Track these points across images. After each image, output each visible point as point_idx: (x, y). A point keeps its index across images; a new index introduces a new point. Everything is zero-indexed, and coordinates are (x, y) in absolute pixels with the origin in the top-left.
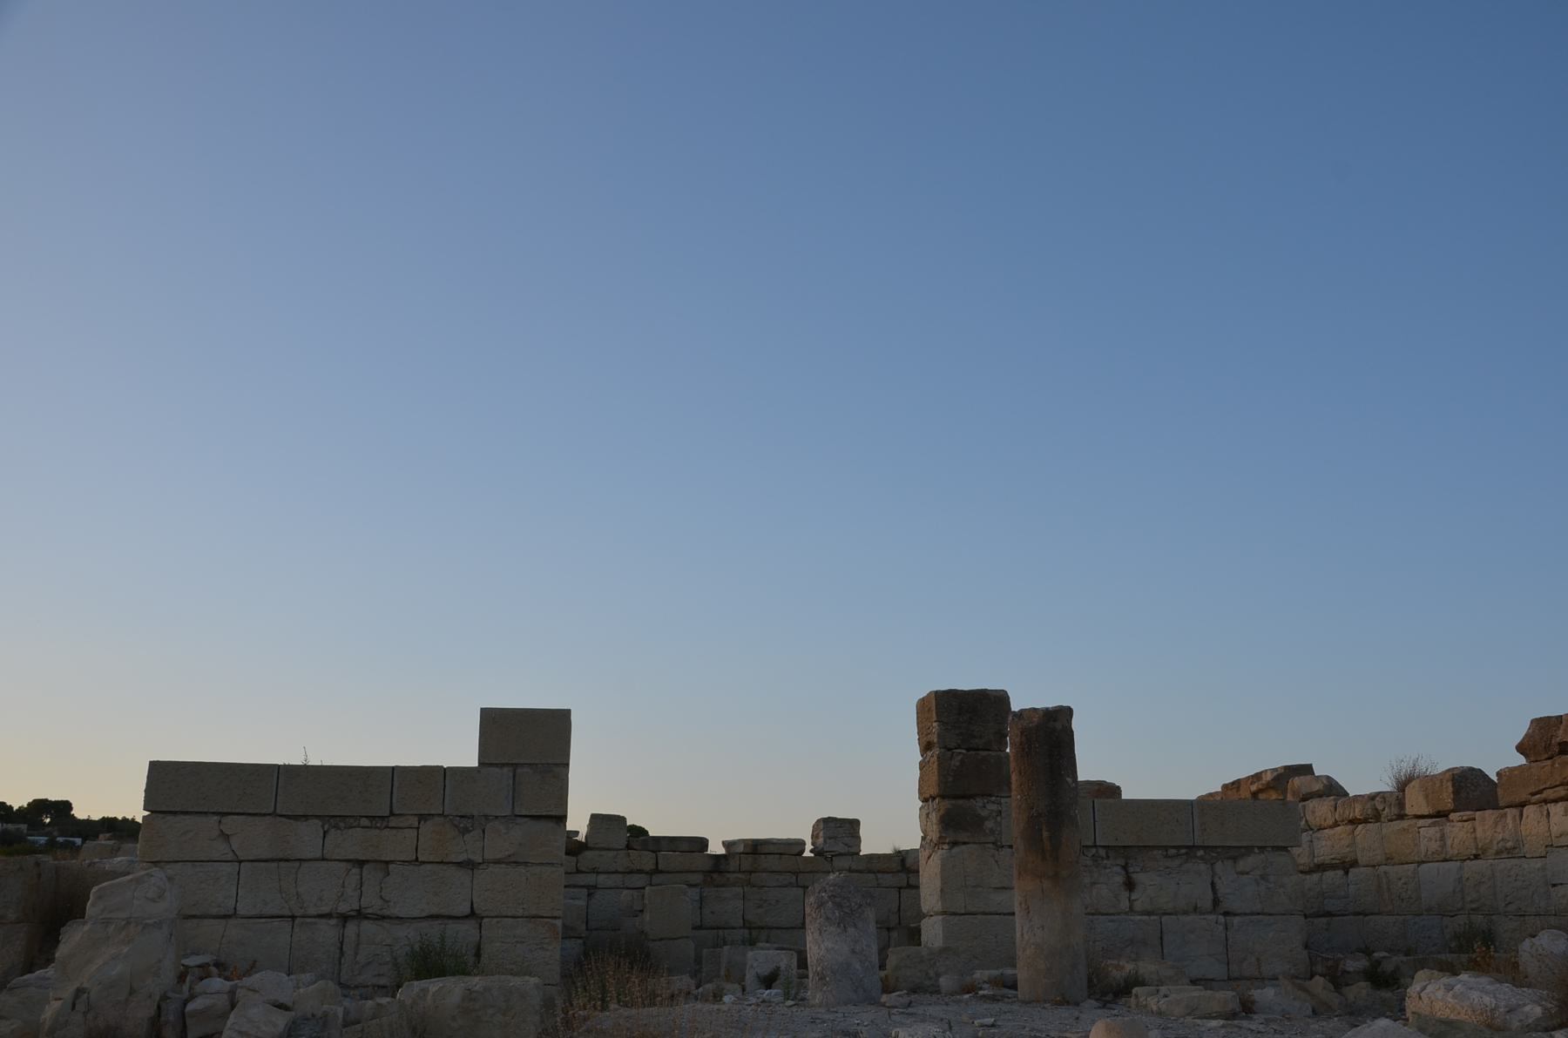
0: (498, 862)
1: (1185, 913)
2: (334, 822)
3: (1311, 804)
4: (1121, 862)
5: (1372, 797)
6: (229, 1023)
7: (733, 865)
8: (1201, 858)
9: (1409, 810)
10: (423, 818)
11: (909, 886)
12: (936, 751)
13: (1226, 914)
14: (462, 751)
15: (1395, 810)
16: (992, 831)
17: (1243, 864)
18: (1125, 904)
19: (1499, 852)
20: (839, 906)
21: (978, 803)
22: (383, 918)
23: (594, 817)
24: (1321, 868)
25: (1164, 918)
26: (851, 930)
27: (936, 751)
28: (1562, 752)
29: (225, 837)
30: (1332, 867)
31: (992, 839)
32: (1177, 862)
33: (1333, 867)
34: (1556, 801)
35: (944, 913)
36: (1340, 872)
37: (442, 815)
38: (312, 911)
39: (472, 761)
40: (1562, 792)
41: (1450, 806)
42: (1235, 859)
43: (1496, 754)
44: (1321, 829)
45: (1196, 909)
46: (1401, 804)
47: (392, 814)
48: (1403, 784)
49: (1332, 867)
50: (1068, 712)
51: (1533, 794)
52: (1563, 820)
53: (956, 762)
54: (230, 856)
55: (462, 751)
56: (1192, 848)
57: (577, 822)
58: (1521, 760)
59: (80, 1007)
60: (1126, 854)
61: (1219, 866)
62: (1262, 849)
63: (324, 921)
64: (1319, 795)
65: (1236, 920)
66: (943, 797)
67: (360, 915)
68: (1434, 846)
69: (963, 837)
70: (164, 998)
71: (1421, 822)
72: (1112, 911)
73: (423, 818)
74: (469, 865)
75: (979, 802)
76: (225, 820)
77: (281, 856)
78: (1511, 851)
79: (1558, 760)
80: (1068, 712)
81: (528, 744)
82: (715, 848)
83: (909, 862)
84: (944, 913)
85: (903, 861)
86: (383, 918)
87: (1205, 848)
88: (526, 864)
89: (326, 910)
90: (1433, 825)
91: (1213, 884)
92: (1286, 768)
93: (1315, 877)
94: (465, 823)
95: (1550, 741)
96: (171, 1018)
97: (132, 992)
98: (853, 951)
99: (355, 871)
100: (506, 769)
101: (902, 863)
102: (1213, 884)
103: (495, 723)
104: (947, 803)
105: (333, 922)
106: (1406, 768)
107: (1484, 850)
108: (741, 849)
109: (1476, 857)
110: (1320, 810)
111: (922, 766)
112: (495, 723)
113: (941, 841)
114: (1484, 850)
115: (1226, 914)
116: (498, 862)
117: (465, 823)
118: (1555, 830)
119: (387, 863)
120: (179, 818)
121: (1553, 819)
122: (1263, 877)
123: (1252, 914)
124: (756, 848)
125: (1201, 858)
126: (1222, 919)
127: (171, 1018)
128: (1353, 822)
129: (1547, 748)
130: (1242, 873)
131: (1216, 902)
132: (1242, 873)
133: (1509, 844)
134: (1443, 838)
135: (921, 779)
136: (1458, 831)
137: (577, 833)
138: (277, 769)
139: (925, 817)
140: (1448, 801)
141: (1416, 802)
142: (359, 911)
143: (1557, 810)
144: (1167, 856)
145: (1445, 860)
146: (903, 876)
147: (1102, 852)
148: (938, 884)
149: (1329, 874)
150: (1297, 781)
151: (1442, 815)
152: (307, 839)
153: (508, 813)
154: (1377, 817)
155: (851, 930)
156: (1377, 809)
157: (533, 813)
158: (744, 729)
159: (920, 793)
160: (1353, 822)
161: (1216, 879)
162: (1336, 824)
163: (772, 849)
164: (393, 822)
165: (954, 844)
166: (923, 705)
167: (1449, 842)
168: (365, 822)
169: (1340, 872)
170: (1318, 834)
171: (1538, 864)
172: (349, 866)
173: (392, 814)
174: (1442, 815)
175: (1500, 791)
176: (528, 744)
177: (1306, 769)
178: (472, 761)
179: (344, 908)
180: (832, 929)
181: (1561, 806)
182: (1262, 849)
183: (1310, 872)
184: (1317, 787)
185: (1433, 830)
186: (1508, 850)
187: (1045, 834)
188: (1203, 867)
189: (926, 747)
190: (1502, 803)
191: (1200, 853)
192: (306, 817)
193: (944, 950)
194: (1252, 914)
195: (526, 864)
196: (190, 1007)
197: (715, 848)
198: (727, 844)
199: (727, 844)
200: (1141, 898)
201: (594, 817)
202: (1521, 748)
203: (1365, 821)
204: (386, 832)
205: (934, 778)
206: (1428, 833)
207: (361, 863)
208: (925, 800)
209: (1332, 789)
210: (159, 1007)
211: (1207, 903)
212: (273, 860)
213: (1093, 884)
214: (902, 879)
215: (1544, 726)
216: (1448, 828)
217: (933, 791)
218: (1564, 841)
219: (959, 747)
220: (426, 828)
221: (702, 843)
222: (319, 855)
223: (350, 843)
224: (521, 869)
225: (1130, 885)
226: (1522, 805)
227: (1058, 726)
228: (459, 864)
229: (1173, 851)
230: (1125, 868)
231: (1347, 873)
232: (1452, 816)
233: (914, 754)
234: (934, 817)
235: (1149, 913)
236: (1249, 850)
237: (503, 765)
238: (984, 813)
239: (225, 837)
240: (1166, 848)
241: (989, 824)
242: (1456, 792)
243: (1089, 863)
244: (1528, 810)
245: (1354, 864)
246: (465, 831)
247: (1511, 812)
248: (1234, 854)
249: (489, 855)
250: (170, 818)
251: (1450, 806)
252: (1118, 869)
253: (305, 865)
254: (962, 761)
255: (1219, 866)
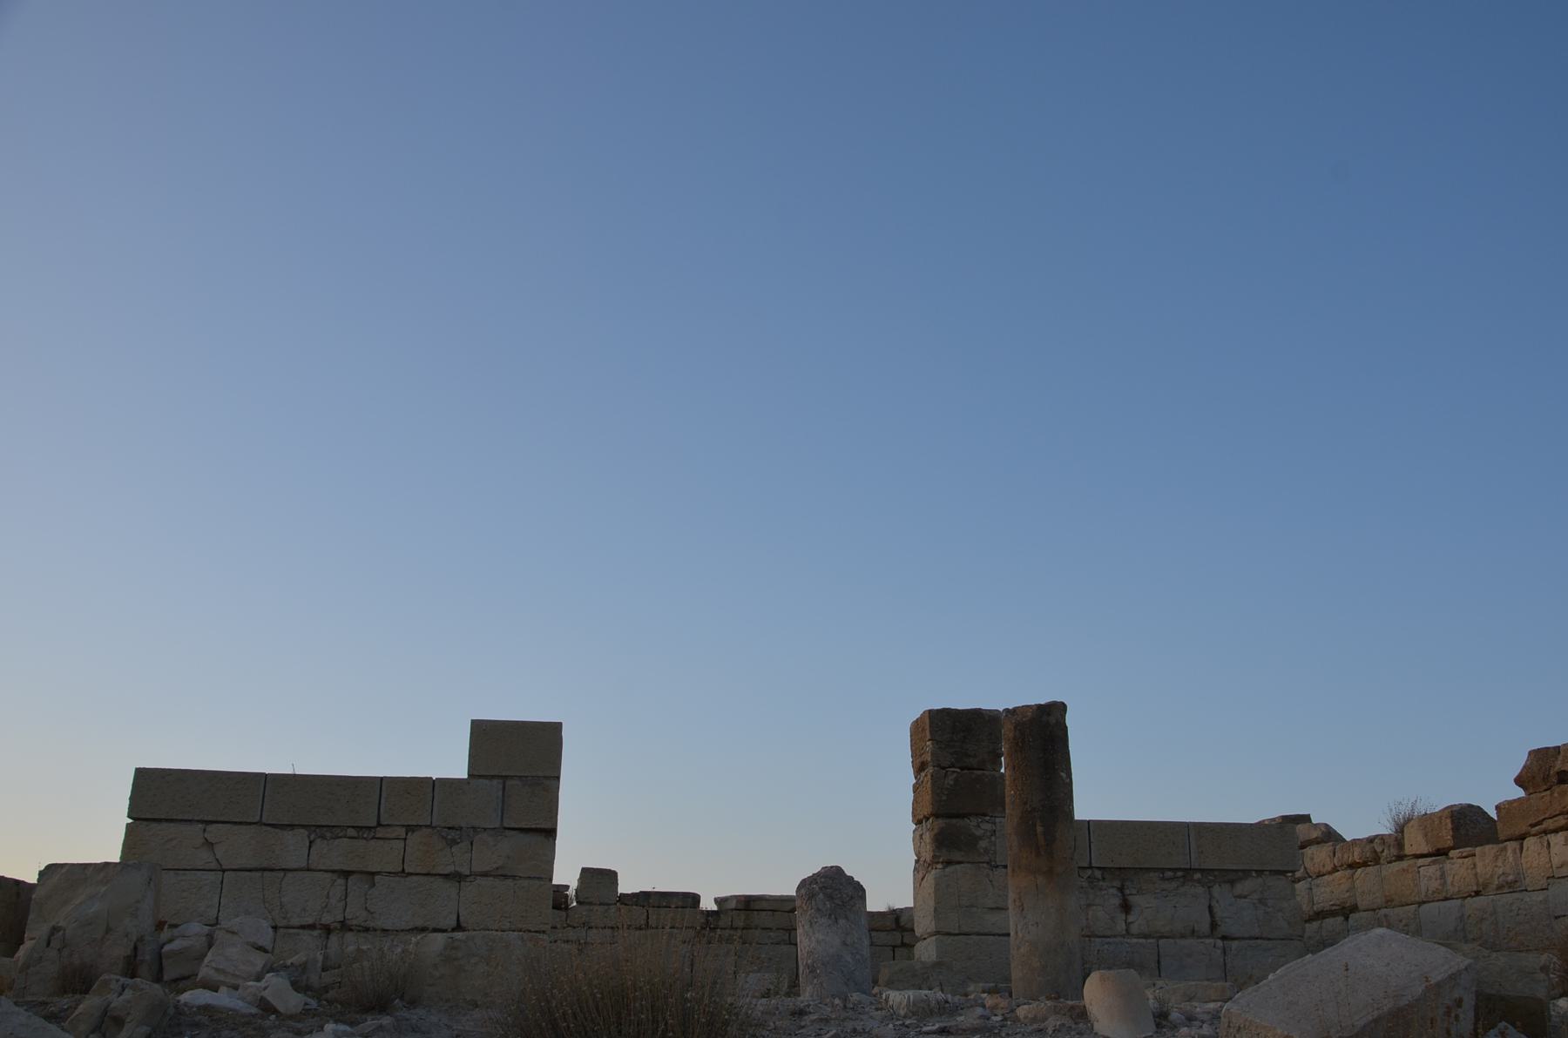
0: (485, 875)
1: (1183, 936)
2: (320, 831)
3: (1308, 851)
4: (1117, 883)
5: (1371, 840)
6: (206, 960)
7: (725, 921)
8: (1199, 881)
9: (1408, 850)
10: (410, 829)
11: (903, 945)
12: (930, 770)
13: (1224, 938)
14: (455, 765)
15: (1394, 851)
16: (986, 851)
17: (1240, 888)
18: (1121, 927)
19: (1500, 887)
20: (830, 898)
21: (972, 822)
22: (367, 930)
23: (584, 871)
24: (1320, 915)
25: (1162, 942)
26: (842, 922)
27: (930, 770)
28: (1561, 781)
29: (209, 845)
30: (1332, 914)
31: (986, 858)
32: (1174, 884)
33: (1332, 914)
34: (1556, 831)
35: (937, 933)
36: (1340, 919)
37: (429, 826)
38: (296, 921)
39: (460, 771)
40: (1562, 821)
41: (1450, 843)
42: (1232, 883)
43: (1493, 788)
44: (1320, 875)
45: (1193, 931)
46: (1400, 844)
47: (379, 824)
48: (1400, 829)
49: (1332, 914)
50: (1060, 708)
51: (1533, 826)
52: (1565, 850)
53: (950, 781)
54: (214, 865)
55: (455, 765)
56: (1188, 872)
57: (566, 874)
58: (1519, 793)
59: (55, 943)
60: (1122, 876)
61: (1216, 890)
62: (1260, 872)
63: (306, 932)
64: (1317, 841)
65: (1235, 944)
66: (936, 815)
67: (345, 926)
68: (1435, 884)
69: (957, 856)
70: (141, 939)
71: (1421, 861)
72: (1108, 933)
73: (410, 829)
74: (457, 877)
75: (973, 822)
76: (211, 828)
77: (265, 865)
78: (1512, 885)
79: (1557, 789)
80: (1060, 708)
81: (520, 760)
82: (708, 904)
83: (903, 920)
84: (937, 933)
85: (897, 920)
86: (367, 930)
87: (1202, 871)
88: (514, 877)
89: (310, 921)
90: (1434, 863)
91: (1210, 908)
92: (1284, 818)
93: (1315, 924)
94: (454, 835)
95: (1549, 772)
96: (148, 957)
97: (108, 930)
98: (844, 944)
99: (341, 881)
100: (495, 782)
101: (896, 921)
102: (1210, 908)
103: (486, 736)
104: (941, 822)
105: (316, 933)
106: (1405, 810)
107: (1485, 886)
108: (733, 905)
109: (1477, 893)
110: (1318, 857)
111: (916, 789)
112: (486, 736)
113: (935, 861)
114: (1485, 886)
115: (1224, 938)
116: (485, 875)
117: (454, 835)
118: (1556, 861)
119: (373, 874)
120: (164, 825)
121: (1554, 850)
122: (1260, 901)
123: (1251, 938)
124: (748, 904)
125: (1199, 881)
126: (1220, 943)
127: (148, 957)
128: (1353, 866)
129: (1546, 779)
130: (1240, 897)
131: (1214, 925)
132: (1240, 897)
133: (1511, 878)
134: (1443, 876)
135: (915, 802)
136: (1458, 869)
137: (567, 887)
138: (265, 777)
139: (918, 838)
140: (1447, 838)
141: (1415, 843)
142: (343, 923)
143: (1557, 840)
144: (1163, 879)
145: (1446, 899)
146: (898, 935)
147: (1098, 874)
148: (932, 903)
149: (1329, 921)
150: (1300, 827)
151: (1441, 853)
152: (292, 849)
153: (497, 825)
154: (1376, 859)
155: (842, 922)
156: (1374, 852)
157: (523, 825)
158: (736, 785)
159: (914, 815)
160: (1353, 866)
161: (1214, 903)
162: (1335, 870)
163: (765, 905)
164: (381, 832)
165: (948, 863)
166: (917, 728)
167: (1449, 880)
168: (351, 832)
169: (1340, 919)
170: (1318, 881)
171: (1540, 896)
172: (335, 876)
173: (379, 824)
174: (1441, 853)
175: (1499, 826)
176: (520, 760)
177: (1305, 819)
178: (460, 771)
179: (327, 919)
180: (824, 920)
181: (1561, 836)
182: (1260, 872)
183: (1310, 920)
184: (1314, 834)
185: (1432, 869)
186: (1510, 884)
187: (1039, 829)
188: (1200, 890)
189: (919, 768)
190: (1502, 837)
191: (1197, 876)
192: (292, 826)
193: (938, 965)
194: (1251, 938)
195: (514, 877)
196: (167, 948)
197: (708, 904)
198: (718, 901)
199: (718, 901)
200: (1138, 922)
201: (584, 871)
202: (1519, 781)
203: (1365, 864)
204: (373, 842)
205: (928, 797)
206: (1429, 872)
207: (346, 874)
208: (918, 822)
209: (1329, 836)
210: (135, 948)
211: (1205, 926)
212: (256, 870)
213: (1089, 905)
214: (896, 938)
215: (1542, 757)
216: (1448, 865)
217: (927, 810)
218: (1564, 871)
219: (953, 766)
220: (414, 838)
221: (694, 899)
222: (304, 864)
223: (335, 854)
224: (509, 882)
225: (1126, 907)
226: (1522, 838)
227: (1052, 720)
228: (446, 876)
229: (1169, 874)
230: (1121, 890)
231: (1347, 919)
232: (1452, 853)
233: (906, 777)
234: (927, 837)
235: (1146, 937)
236: (1246, 873)
237: (493, 777)
238: (978, 833)
239: (209, 845)
240: (1163, 870)
241: (983, 844)
242: (1455, 829)
243: (1085, 884)
244: (1529, 842)
245: (1354, 909)
246: (453, 842)
247: (1511, 845)
248: (1231, 877)
249: (477, 868)
250: (154, 825)
251: (1450, 843)
252: (1114, 891)
253: (290, 875)
254: (956, 780)
255: (1216, 890)
